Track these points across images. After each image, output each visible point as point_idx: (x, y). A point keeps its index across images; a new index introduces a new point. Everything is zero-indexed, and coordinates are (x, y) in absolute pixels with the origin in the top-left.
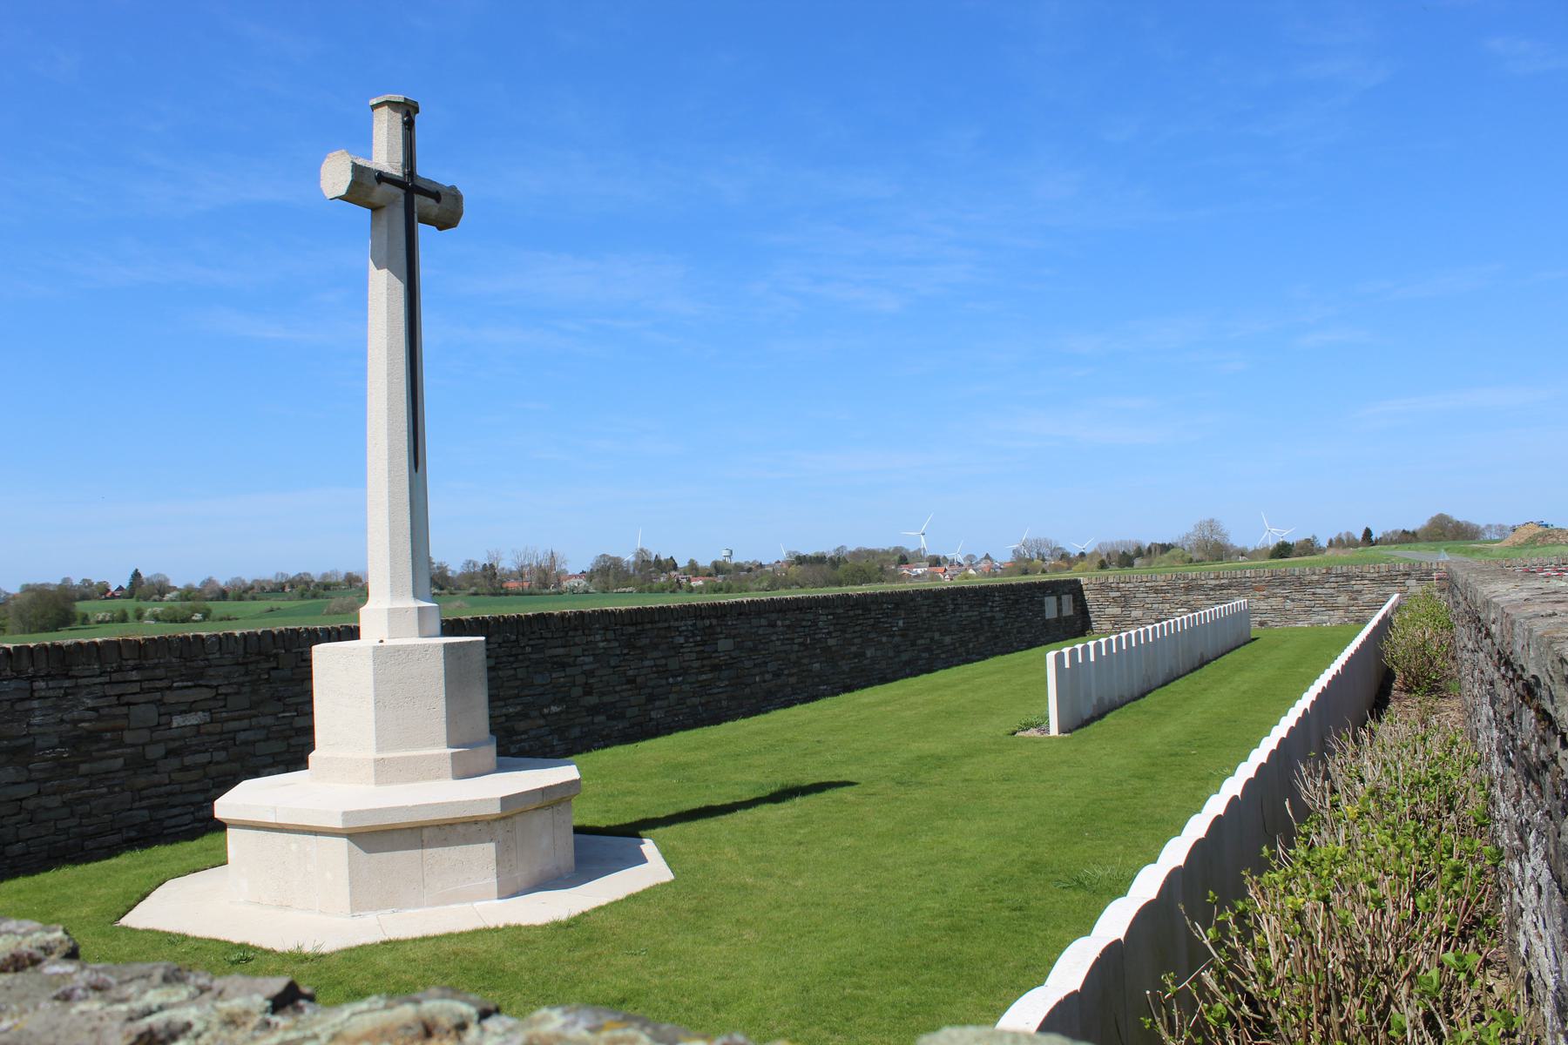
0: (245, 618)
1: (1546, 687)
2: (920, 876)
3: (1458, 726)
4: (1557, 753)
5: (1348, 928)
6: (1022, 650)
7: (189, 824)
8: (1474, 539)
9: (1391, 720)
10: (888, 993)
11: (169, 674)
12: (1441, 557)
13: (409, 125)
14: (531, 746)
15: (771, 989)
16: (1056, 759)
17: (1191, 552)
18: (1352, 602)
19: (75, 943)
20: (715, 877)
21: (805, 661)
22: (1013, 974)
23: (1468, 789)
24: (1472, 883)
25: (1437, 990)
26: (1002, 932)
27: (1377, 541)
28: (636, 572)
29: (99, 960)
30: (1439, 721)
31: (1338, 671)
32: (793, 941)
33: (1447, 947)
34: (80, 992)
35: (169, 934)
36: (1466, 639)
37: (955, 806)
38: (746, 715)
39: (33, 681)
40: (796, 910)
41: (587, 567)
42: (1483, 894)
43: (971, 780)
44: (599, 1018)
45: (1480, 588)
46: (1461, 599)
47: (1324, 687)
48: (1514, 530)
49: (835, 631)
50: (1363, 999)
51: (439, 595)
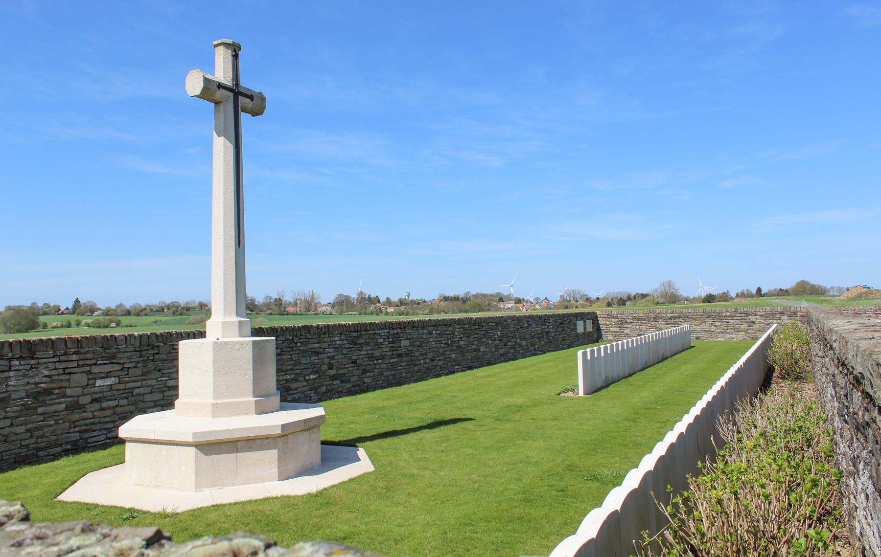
0: (141, 326)
1: (868, 379)
2: (508, 471)
3: (813, 399)
4: (875, 417)
5: (749, 511)
6: (564, 349)
7: (103, 440)
8: (823, 294)
9: (772, 394)
10: (490, 536)
11: (95, 357)
12: (803, 304)
13: (235, 57)
14: (299, 397)
15: (427, 532)
16: (582, 409)
17: (658, 298)
18: (750, 328)
19: (28, 512)
20: (397, 469)
21: (448, 353)
22: (558, 527)
23: (820, 435)
24: (824, 490)
25: (805, 551)
26: (553, 504)
27: (764, 294)
28: (358, 304)
29: (43, 521)
30: (801, 396)
31: (741, 365)
32: (438, 505)
33: (810, 526)
34: (28, 541)
35: (87, 504)
36: (817, 351)
37: (527, 433)
38: (415, 381)
39: (10, 361)
40: (440, 488)
41: (331, 301)
42: (831, 497)
43: (536, 419)
44: (331, 548)
45: (827, 322)
46: (814, 328)
47: (733, 374)
48: (848, 290)
49: (464, 337)
50: (759, 553)
51: (251, 314)
